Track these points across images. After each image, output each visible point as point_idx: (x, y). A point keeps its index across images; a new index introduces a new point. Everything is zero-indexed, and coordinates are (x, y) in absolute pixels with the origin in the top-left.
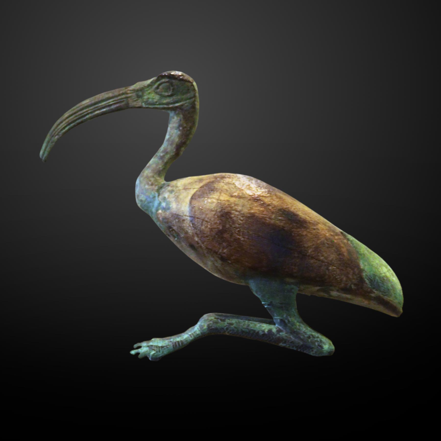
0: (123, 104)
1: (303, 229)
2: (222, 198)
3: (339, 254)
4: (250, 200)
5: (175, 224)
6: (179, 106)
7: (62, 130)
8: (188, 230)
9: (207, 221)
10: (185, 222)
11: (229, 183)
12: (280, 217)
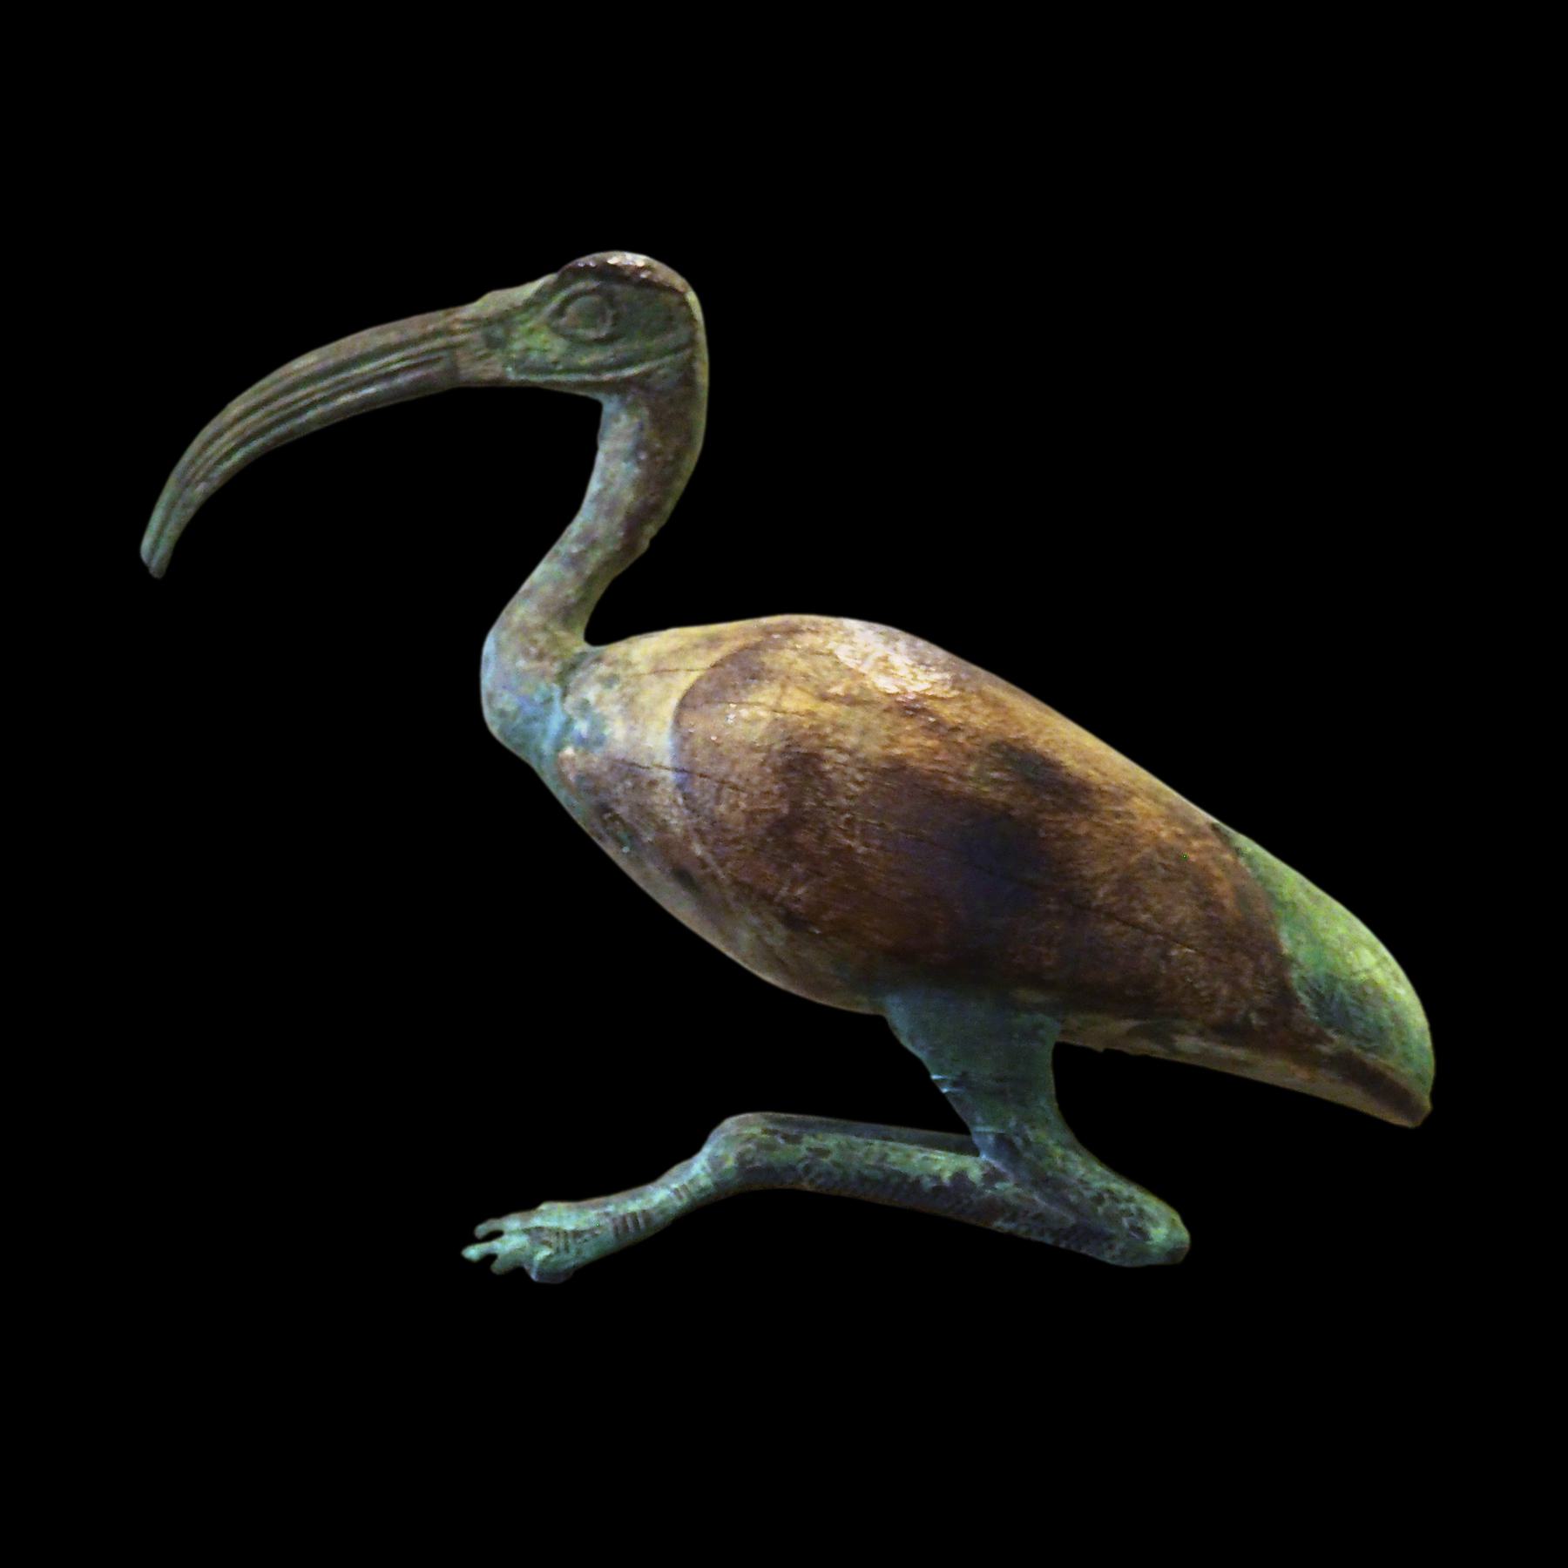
0: (437, 368)
1: (1076, 815)
2: (788, 704)
3: (1207, 905)
4: (888, 710)
5: (621, 796)
6: (636, 376)
7: (220, 462)
8: (667, 818)
9: (735, 787)
10: (658, 790)
11: (813, 652)
12: (995, 770)
